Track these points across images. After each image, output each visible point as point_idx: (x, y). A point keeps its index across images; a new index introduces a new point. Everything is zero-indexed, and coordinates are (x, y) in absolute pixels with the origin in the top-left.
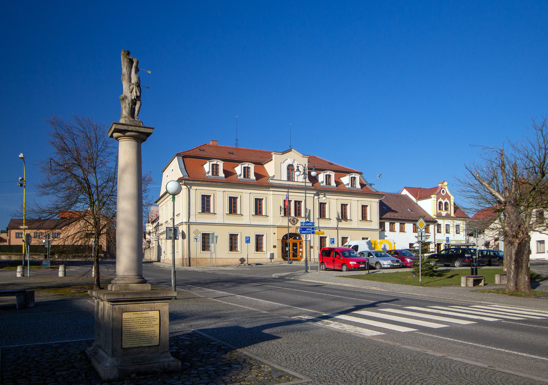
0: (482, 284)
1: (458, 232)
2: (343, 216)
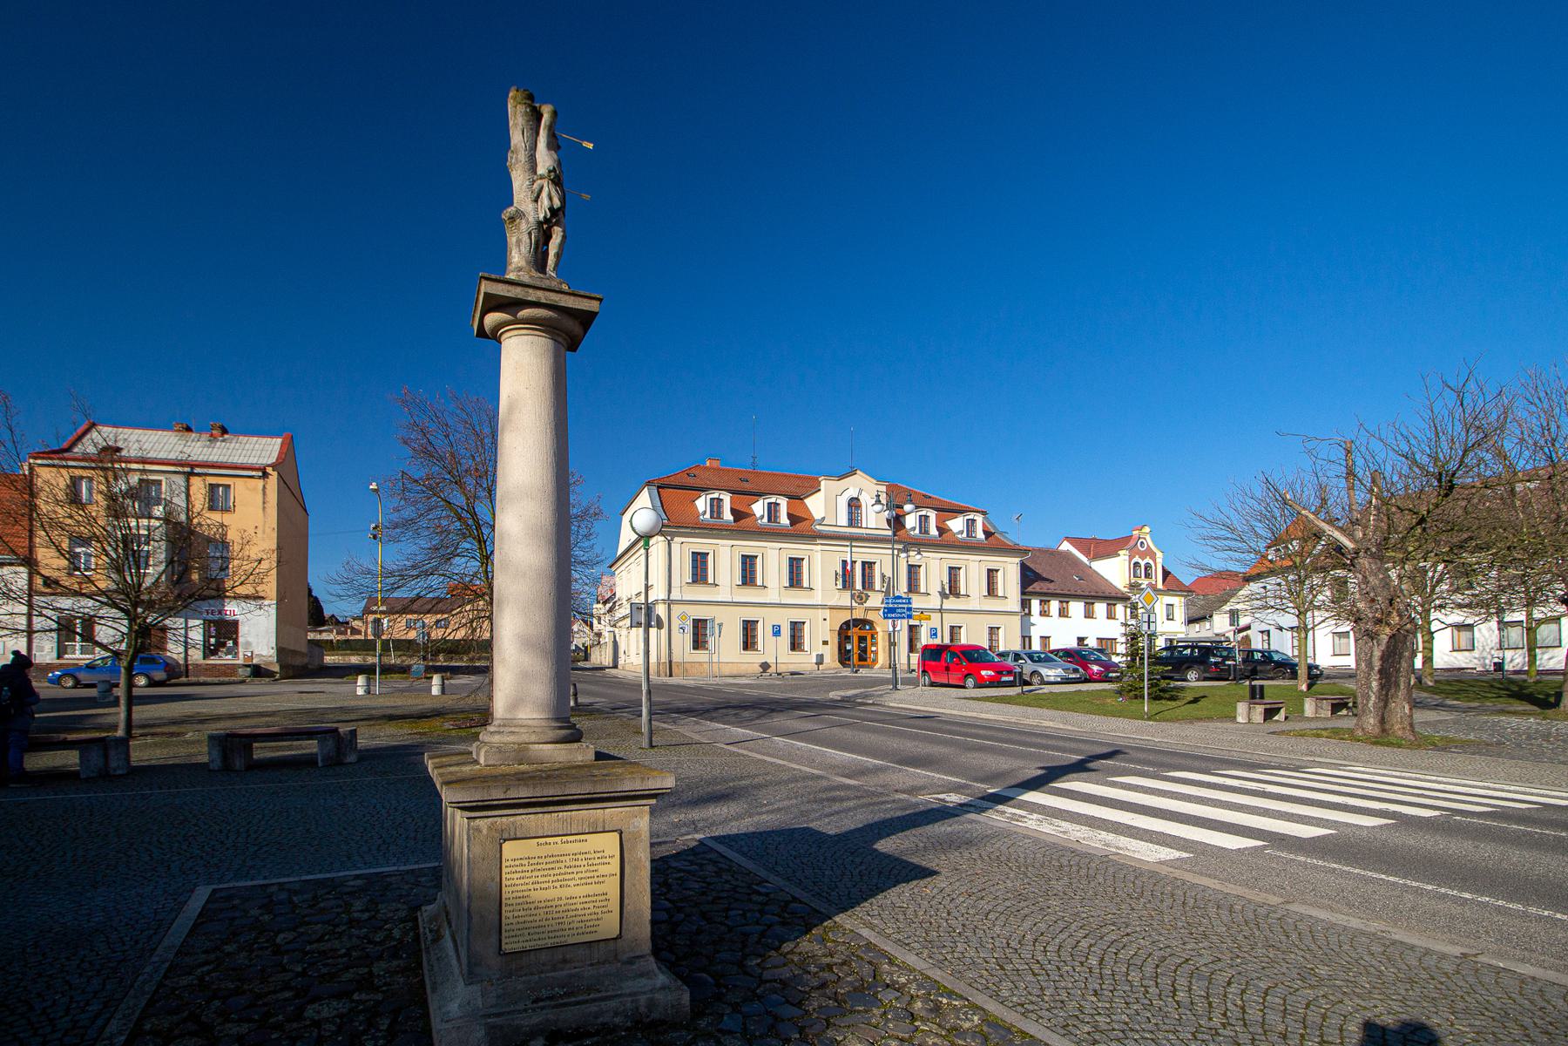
0: (1280, 716)
1: (1170, 618)
2: (952, 589)
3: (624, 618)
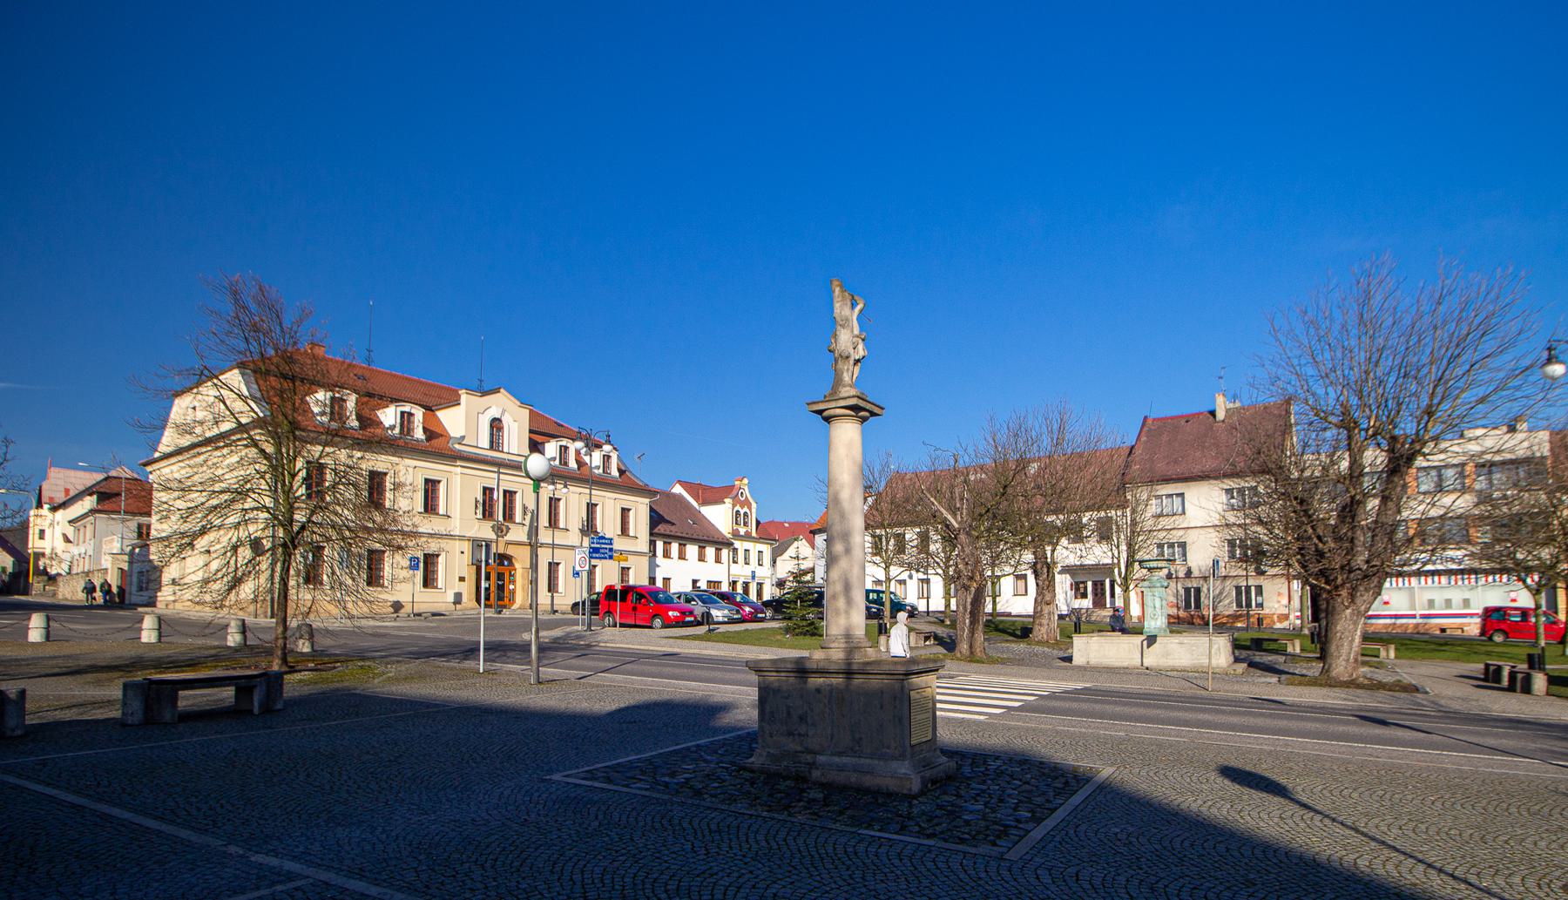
3: (187, 541)
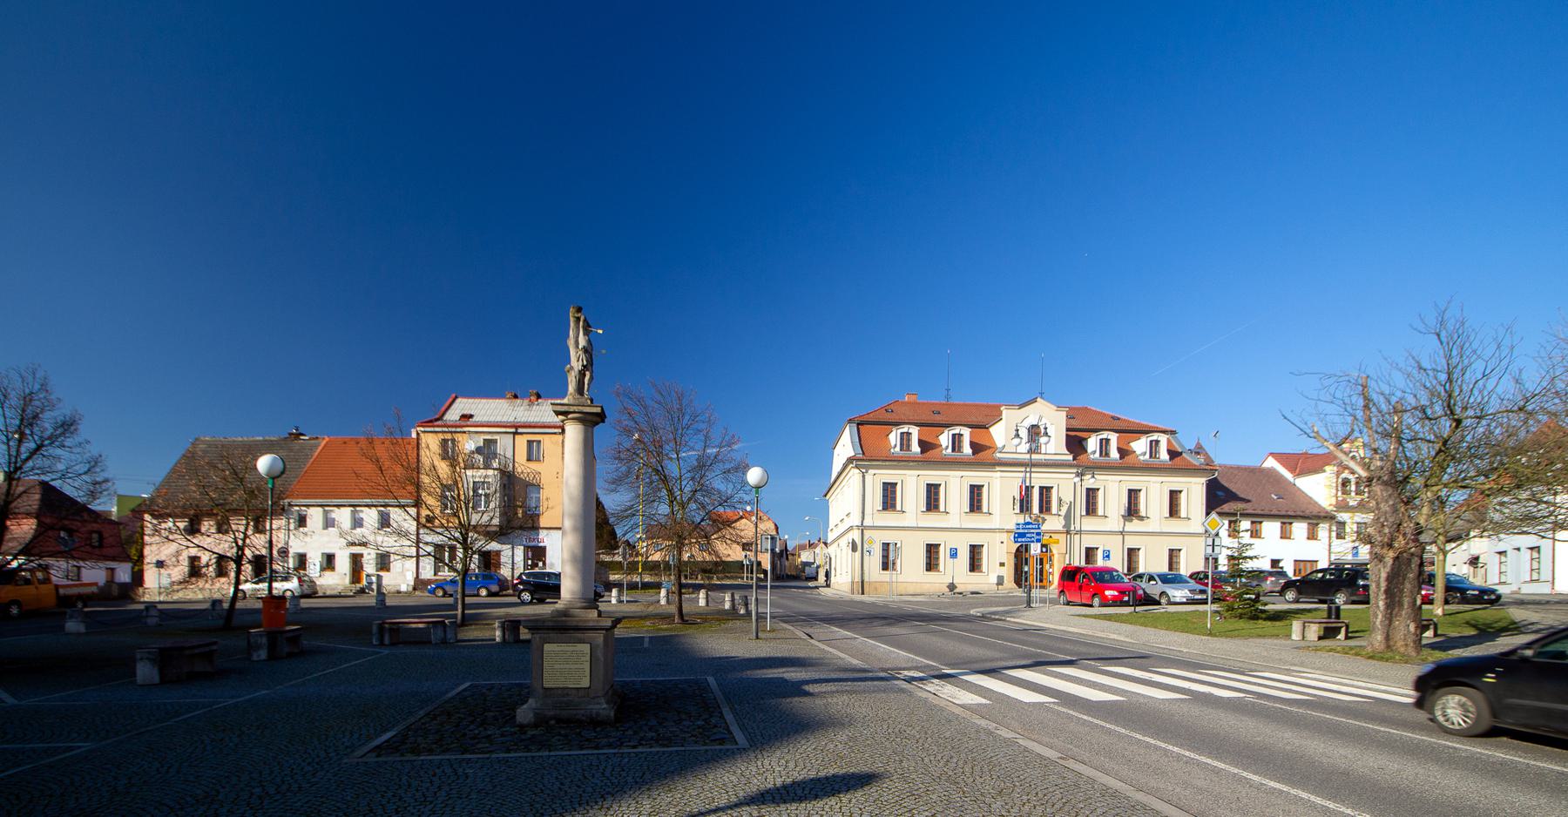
0: (1341, 636)
2: (1132, 511)
